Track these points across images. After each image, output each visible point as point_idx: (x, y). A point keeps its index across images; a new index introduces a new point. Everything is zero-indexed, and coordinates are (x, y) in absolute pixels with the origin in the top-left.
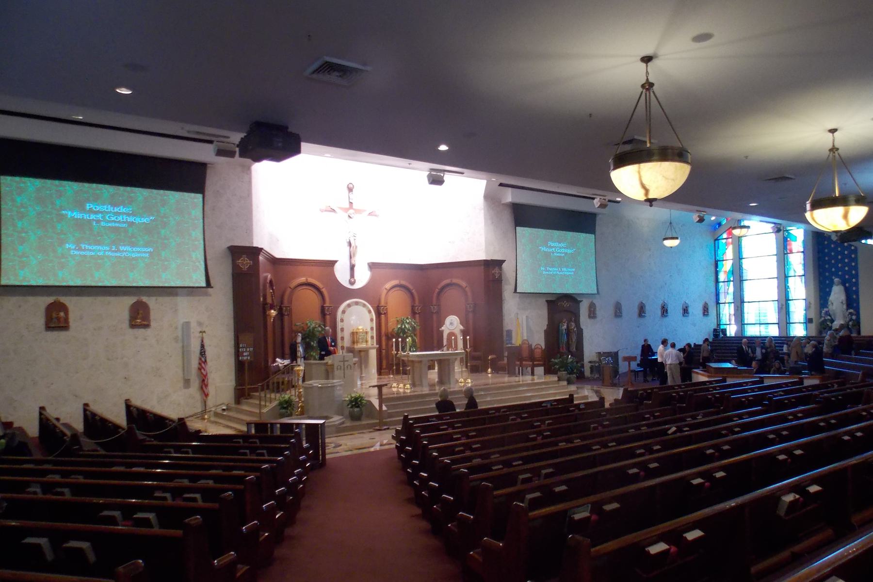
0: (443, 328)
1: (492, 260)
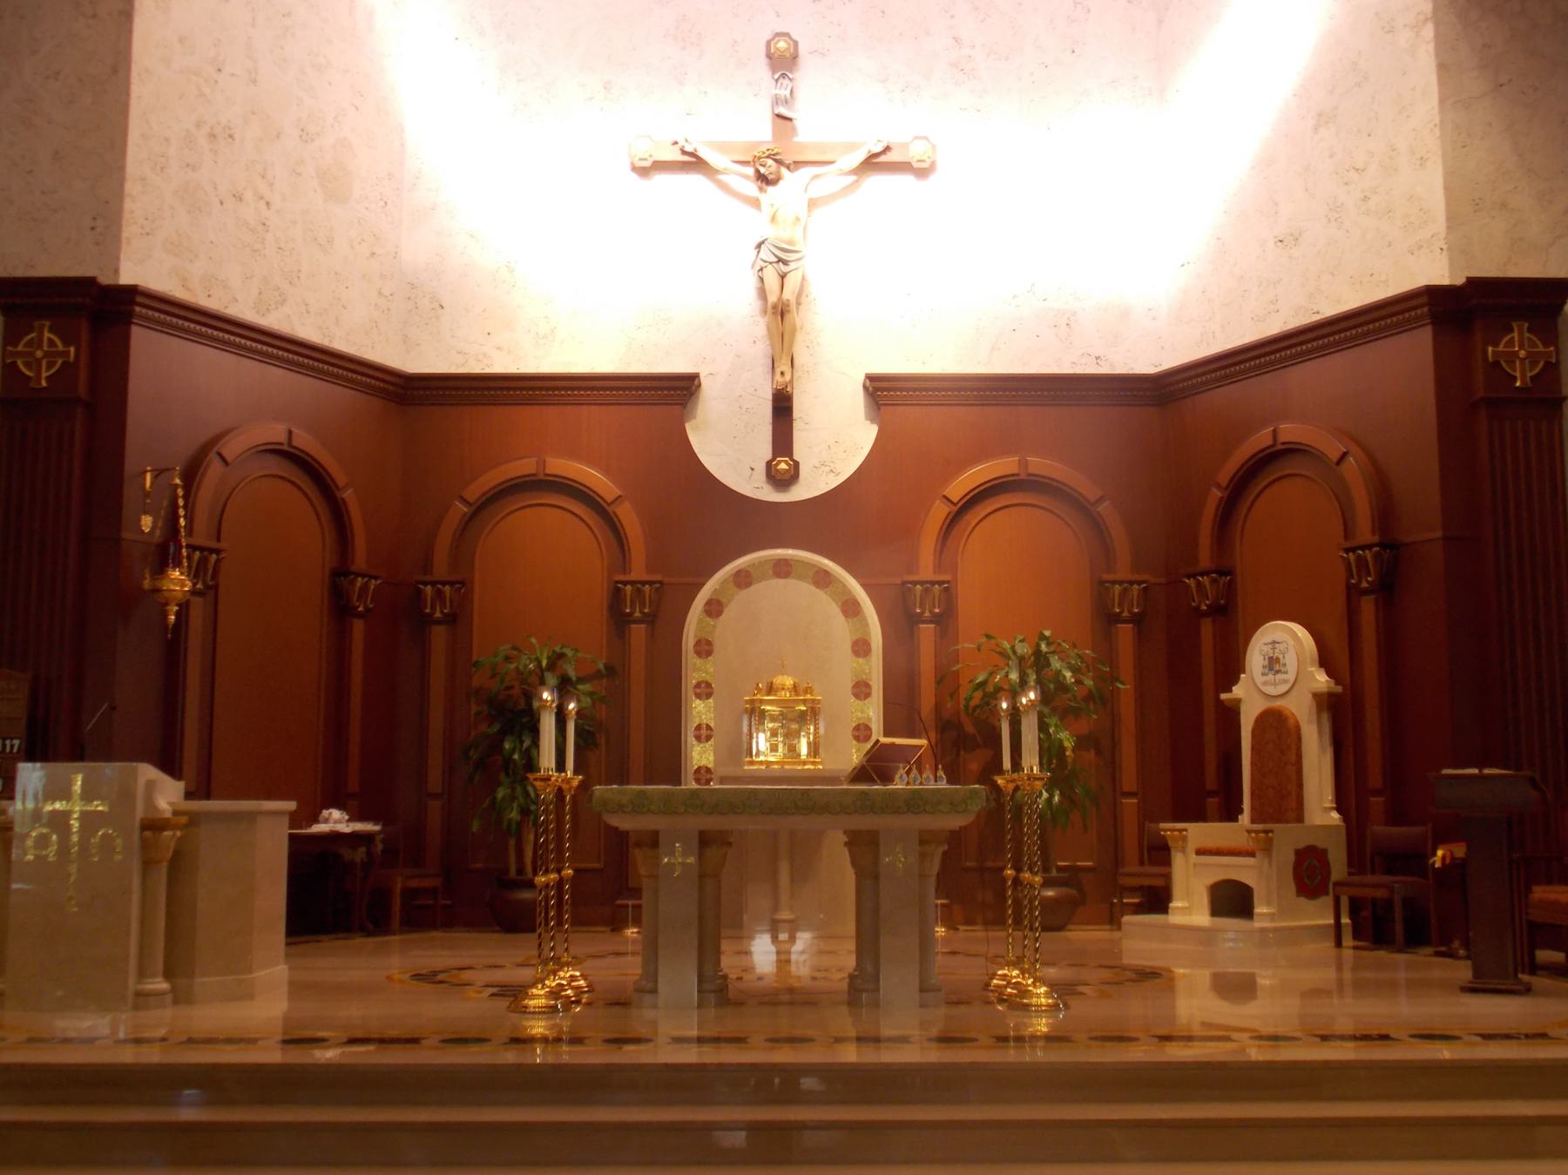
0: (1238, 691)
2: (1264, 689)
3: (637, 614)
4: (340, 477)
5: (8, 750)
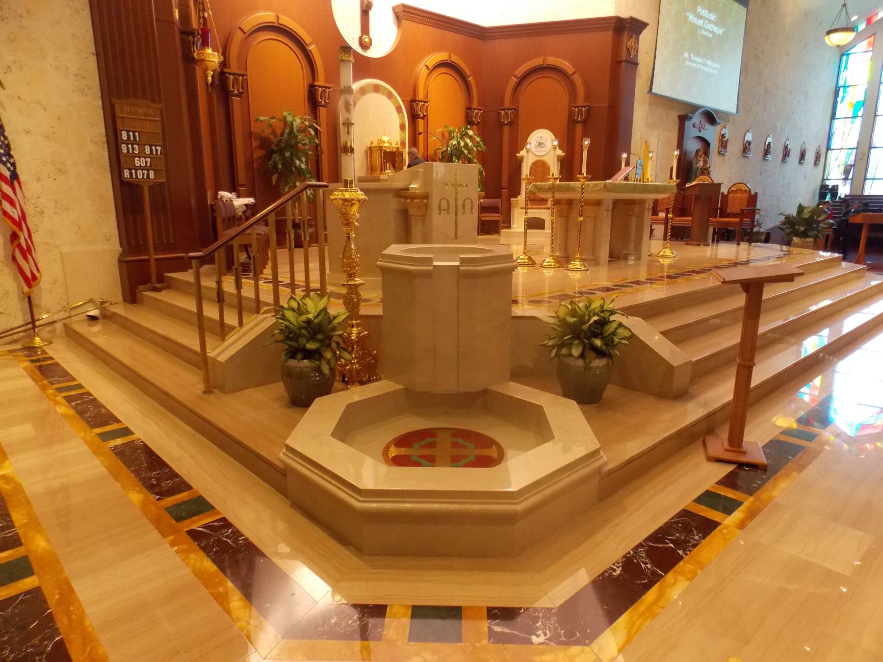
0: (523, 153)
1: (632, 18)
2: (536, 153)
3: (236, 92)
4: (306, 38)
5: (154, 153)
